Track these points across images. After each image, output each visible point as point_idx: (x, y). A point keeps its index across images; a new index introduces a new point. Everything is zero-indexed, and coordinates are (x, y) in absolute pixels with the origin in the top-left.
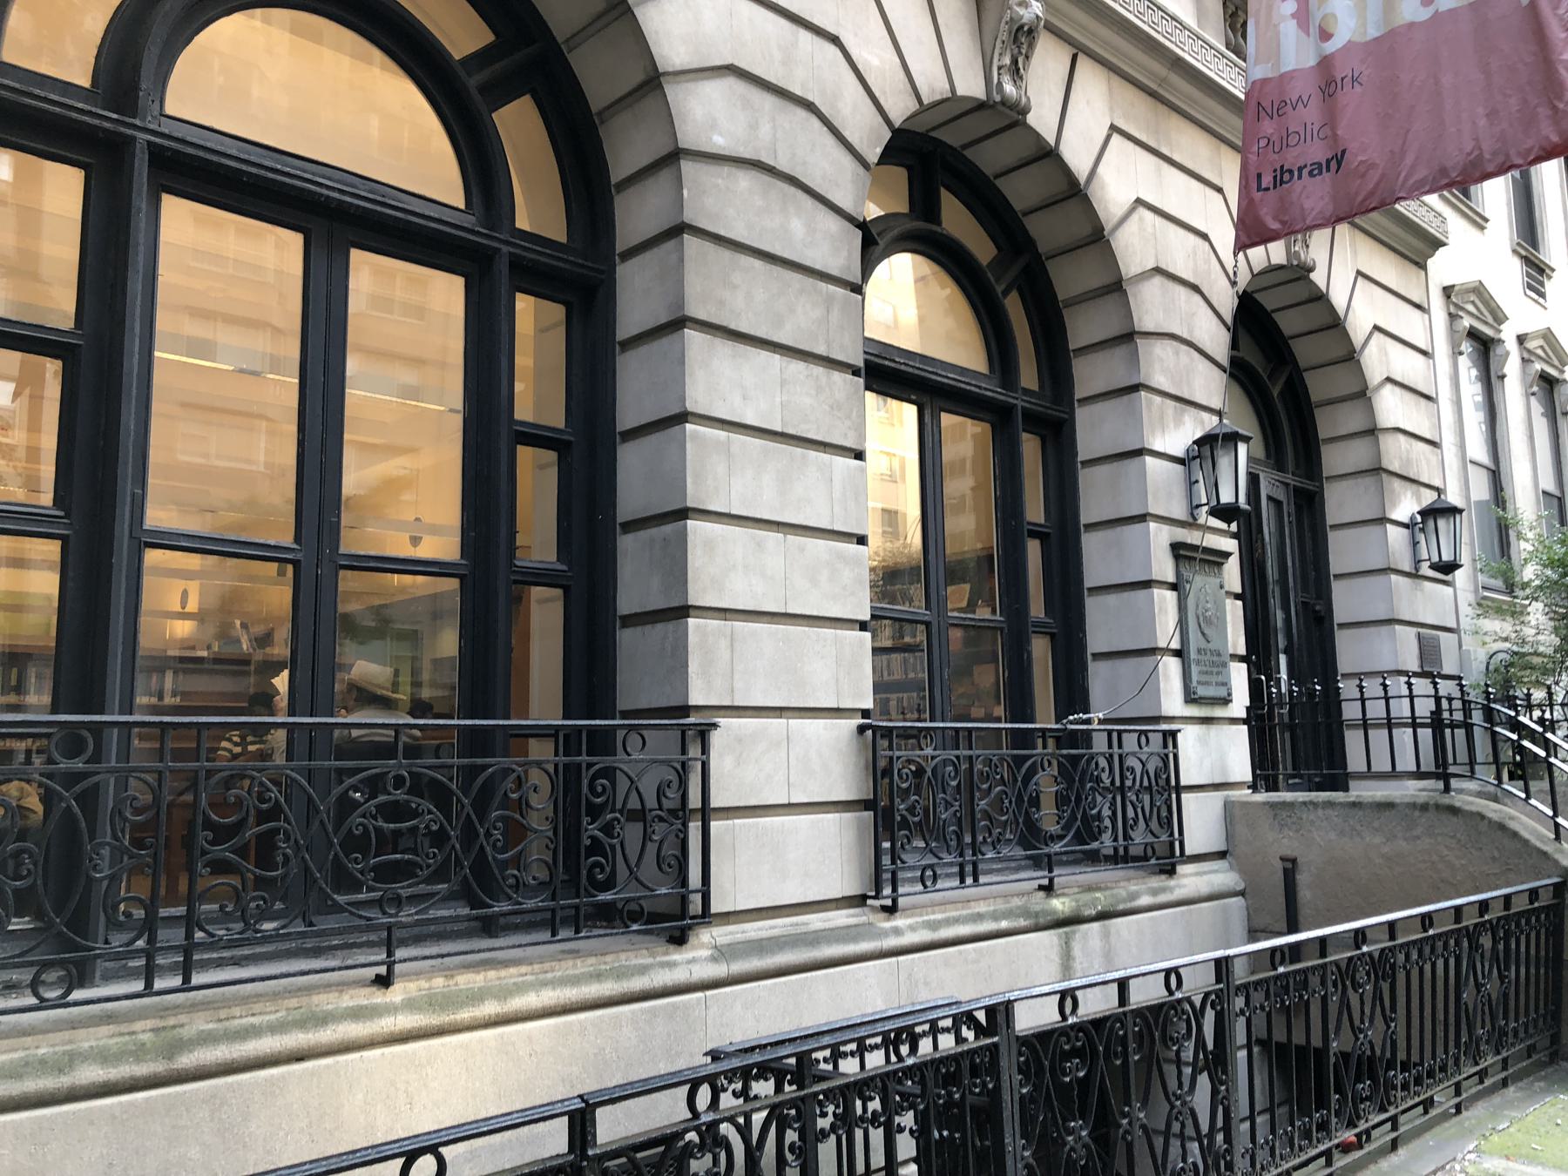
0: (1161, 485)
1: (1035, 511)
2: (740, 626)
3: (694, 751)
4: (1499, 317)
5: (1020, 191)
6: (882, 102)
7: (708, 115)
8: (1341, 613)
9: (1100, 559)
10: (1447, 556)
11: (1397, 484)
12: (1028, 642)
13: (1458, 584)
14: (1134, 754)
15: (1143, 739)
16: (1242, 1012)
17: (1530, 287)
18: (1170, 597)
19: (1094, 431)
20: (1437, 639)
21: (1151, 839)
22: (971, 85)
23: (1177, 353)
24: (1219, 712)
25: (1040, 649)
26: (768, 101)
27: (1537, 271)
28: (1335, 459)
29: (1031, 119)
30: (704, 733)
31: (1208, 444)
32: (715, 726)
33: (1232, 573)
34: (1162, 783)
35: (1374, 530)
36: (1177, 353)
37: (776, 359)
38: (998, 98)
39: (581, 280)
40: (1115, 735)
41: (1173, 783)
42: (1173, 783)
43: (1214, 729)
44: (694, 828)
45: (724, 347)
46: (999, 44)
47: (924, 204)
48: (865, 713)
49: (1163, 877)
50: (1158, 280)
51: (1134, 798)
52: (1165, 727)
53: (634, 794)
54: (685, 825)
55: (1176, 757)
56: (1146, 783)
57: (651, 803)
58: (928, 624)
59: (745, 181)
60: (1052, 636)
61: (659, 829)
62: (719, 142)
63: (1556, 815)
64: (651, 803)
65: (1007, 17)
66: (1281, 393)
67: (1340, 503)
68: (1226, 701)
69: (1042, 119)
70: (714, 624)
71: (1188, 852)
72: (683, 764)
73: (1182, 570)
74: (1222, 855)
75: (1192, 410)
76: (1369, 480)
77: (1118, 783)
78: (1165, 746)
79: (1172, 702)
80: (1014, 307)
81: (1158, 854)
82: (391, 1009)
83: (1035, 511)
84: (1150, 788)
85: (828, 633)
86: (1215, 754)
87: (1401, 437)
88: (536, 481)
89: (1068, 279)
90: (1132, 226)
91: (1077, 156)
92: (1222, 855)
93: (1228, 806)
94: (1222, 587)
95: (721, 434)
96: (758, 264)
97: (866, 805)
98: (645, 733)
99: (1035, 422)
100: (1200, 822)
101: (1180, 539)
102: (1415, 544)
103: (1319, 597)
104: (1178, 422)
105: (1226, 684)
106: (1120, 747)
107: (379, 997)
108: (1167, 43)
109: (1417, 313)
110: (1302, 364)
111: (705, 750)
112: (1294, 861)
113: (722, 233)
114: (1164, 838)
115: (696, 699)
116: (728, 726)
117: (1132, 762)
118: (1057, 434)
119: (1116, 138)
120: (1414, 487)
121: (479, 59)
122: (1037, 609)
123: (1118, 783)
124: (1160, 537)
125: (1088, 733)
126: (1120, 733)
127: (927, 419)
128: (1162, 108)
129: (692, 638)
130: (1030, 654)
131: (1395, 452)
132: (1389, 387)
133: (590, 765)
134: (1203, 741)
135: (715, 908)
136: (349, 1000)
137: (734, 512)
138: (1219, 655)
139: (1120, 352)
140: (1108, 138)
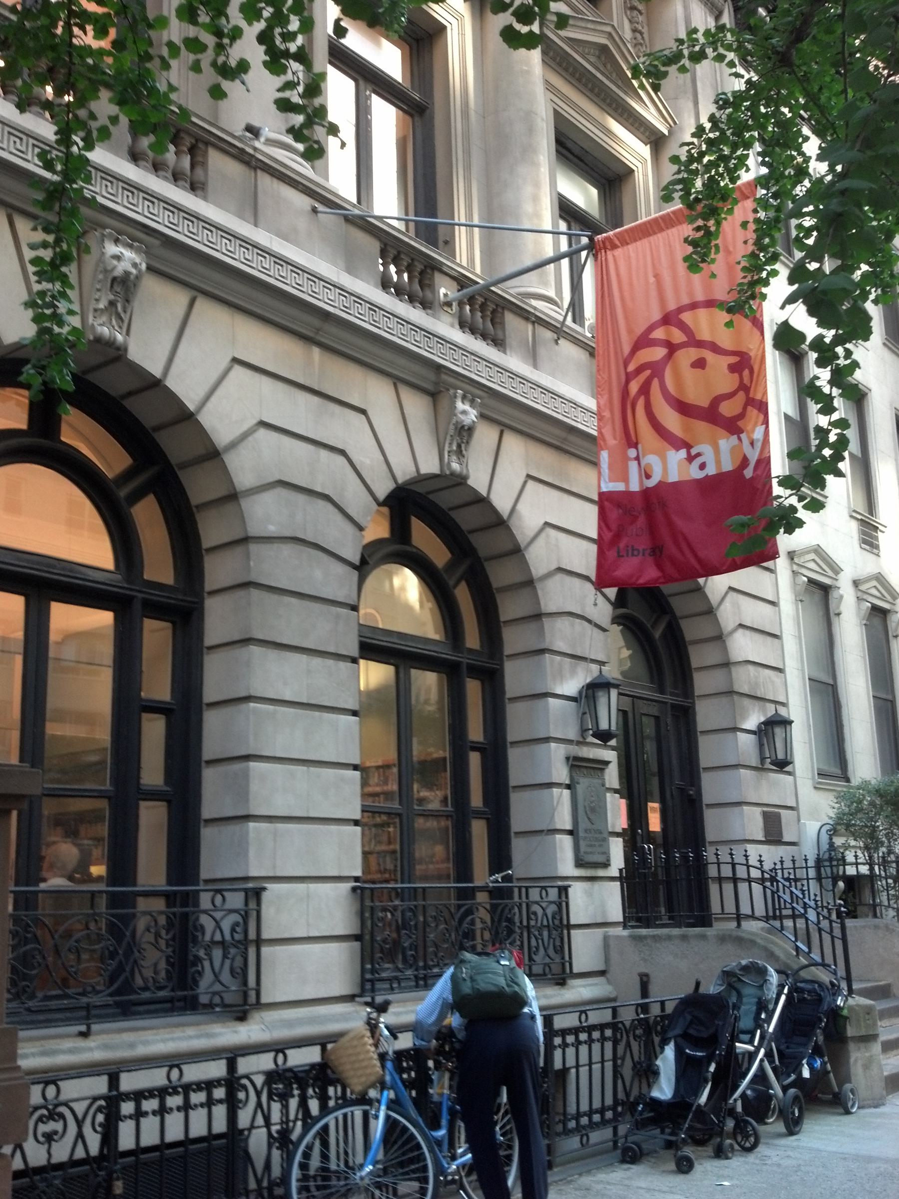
0: (559, 719)
1: (476, 732)
2: (281, 826)
3: (252, 905)
4: (836, 570)
5: (466, 519)
6: (372, 487)
7: (266, 514)
8: (708, 797)
9: (519, 767)
10: (781, 756)
11: (746, 702)
12: (470, 825)
13: (798, 773)
14: (537, 903)
15: (544, 893)
16: (560, 1046)
17: (864, 542)
18: (566, 793)
19: (516, 677)
20: (778, 816)
21: (547, 960)
22: (430, 465)
23: (573, 625)
24: (601, 873)
25: (479, 830)
26: (301, 498)
27: (869, 533)
28: (702, 683)
29: (470, 482)
30: (257, 893)
31: (594, 688)
32: (264, 889)
33: (612, 777)
34: (557, 922)
35: (729, 736)
36: (573, 625)
37: (304, 658)
38: (448, 472)
39: (183, 612)
40: (524, 890)
41: (565, 922)
42: (565, 922)
43: (597, 885)
44: (252, 951)
45: (273, 654)
46: (449, 438)
47: (400, 529)
48: (357, 879)
49: (557, 987)
50: (559, 577)
51: (536, 933)
52: (560, 883)
53: (218, 932)
54: (246, 949)
55: (259, 913)
56: (545, 923)
57: (228, 937)
58: (399, 815)
59: (286, 550)
60: (487, 819)
61: (233, 951)
62: (272, 529)
63: (796, 940)
64: (228, 937)
65: (454, 421)
66: (664, 635)
67: (707, 714)
68: (606, 865)
69: (478, 481)
70: (264, 826)
71: (575, 970)
72: (246, 912)
73: (574, 774)
74: (602, 973)
75: (583, 664)
76: (724, 700)
77: (525, 923)
78: (560, 897)
79: (566, 866)
80: (463, 595)
81: (554, 971)
82: (91, 1049)
83: (476, 732)
84: (548, 926)
85: (334, 828)
86: (597, 902)
87: (751, 668)
88: (154, 732)
89: (500, 575)
90: (541, 541)
91: (502, 502)
92: (602, 973)
93: (606, 939)
94: (603, 785)
95: (271, 708)
96: (293, 601)
97: (357, 938)
98: (225, 894)
99: (476, 672)
100: (584, 950)
101: (573, 754)
102: (761, 746)
103: (692, 785)
104: (573, 672)
105: (607, 854)
106: (527, 897)
107: (81, 1043)
108: (565, 420)
109: (768, 573)
110: (678, 613)
111: (259, 903)
112: (647, 975)
113: (273, 584)
114: (558, 959)
115: (254, 873)
116: (273, 888)
117: (535, 908)
118: (492, 678)
119: (531, 483)
120: (762, 703)
121: (127, 476)
122: (476, 800)
123: (525, 923)
124: (557, 753)
125: (511, 889)
126: (527, 888)
127: (402, 675)
128: (567, 457)
129: (252, 835)
130: (470, 833)
131: (743, 679)
132: (740, 631)
133: (459, 907)
134: (589, 894)
135: (264, 999)
136: (68, 1044)
137: (278, 755)
138: (601, 833)
139: (533, 626)
140: (525, 483)
